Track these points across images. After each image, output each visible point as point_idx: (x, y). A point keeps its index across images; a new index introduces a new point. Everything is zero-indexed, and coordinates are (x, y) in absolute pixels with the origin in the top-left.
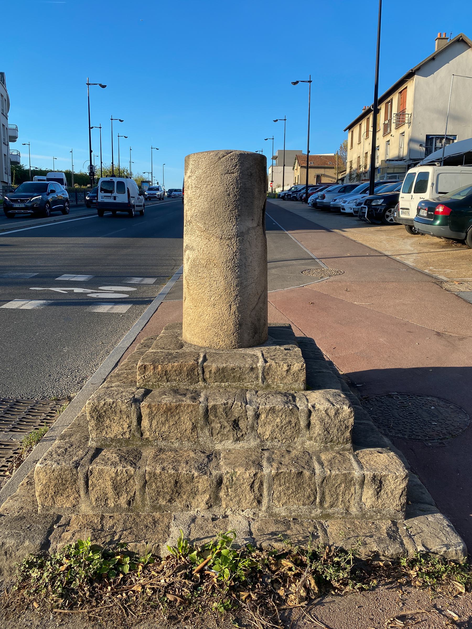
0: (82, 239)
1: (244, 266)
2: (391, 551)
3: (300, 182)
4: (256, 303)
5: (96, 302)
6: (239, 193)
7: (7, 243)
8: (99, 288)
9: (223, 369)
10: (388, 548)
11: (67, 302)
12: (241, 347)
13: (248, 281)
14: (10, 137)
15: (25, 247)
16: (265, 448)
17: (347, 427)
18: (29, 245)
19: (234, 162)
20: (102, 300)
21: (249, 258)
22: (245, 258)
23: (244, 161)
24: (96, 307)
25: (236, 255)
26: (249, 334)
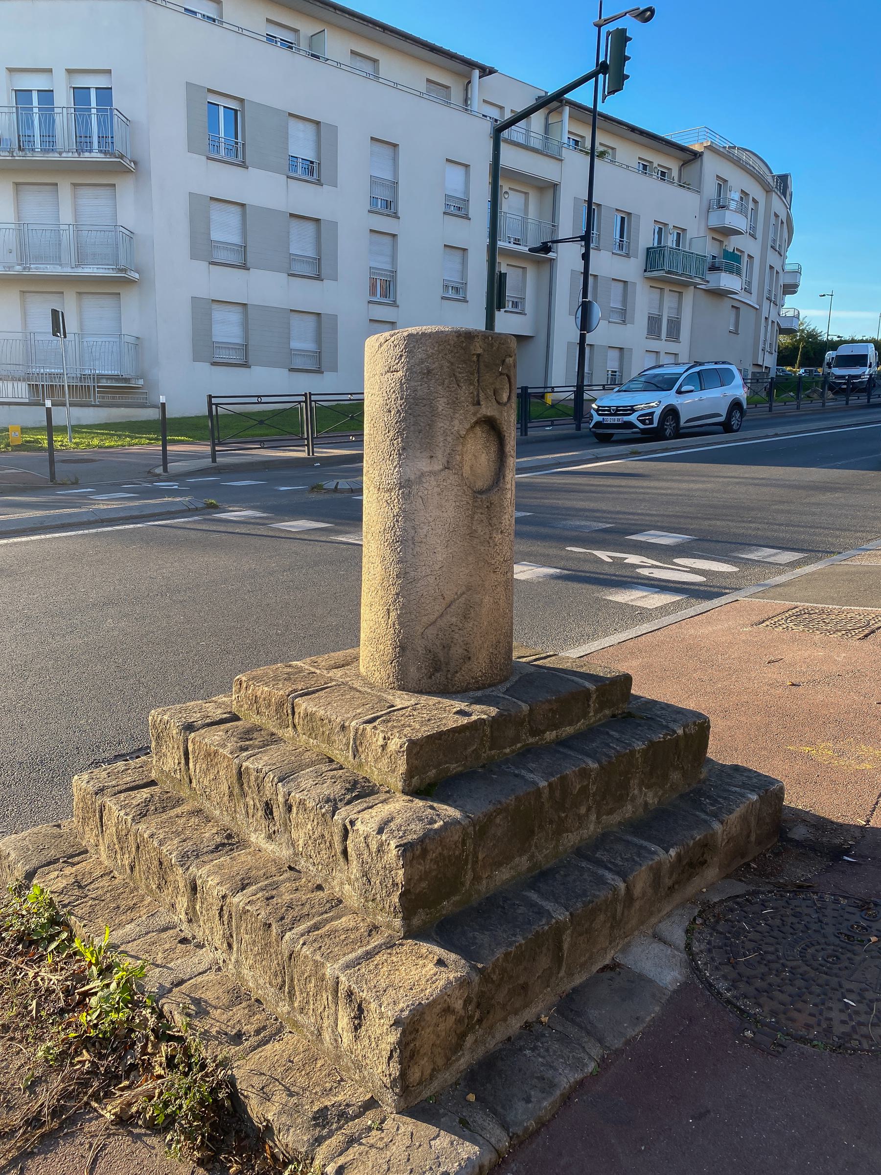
0: (789, 469)
1: (410, 542)
2: (289, 1138)
4: (437, 614)
5: (630, 582)
6: (405, 407)
7: (641, 471)
8: (675, 560)
9: (313, 714)
10: (288, 1130)
11: (585, 577)
12: (403, 689)
14: (785, 286)
15: (667, 480)
16: (297, 868)
17: (395, 884)
18: (669, 478)
19: (398, 350)
20: (646, 582)
21: (422, 529)
22: (414, 528)
23: (414, 347)
25: (397, 521)
26: (419, 669)
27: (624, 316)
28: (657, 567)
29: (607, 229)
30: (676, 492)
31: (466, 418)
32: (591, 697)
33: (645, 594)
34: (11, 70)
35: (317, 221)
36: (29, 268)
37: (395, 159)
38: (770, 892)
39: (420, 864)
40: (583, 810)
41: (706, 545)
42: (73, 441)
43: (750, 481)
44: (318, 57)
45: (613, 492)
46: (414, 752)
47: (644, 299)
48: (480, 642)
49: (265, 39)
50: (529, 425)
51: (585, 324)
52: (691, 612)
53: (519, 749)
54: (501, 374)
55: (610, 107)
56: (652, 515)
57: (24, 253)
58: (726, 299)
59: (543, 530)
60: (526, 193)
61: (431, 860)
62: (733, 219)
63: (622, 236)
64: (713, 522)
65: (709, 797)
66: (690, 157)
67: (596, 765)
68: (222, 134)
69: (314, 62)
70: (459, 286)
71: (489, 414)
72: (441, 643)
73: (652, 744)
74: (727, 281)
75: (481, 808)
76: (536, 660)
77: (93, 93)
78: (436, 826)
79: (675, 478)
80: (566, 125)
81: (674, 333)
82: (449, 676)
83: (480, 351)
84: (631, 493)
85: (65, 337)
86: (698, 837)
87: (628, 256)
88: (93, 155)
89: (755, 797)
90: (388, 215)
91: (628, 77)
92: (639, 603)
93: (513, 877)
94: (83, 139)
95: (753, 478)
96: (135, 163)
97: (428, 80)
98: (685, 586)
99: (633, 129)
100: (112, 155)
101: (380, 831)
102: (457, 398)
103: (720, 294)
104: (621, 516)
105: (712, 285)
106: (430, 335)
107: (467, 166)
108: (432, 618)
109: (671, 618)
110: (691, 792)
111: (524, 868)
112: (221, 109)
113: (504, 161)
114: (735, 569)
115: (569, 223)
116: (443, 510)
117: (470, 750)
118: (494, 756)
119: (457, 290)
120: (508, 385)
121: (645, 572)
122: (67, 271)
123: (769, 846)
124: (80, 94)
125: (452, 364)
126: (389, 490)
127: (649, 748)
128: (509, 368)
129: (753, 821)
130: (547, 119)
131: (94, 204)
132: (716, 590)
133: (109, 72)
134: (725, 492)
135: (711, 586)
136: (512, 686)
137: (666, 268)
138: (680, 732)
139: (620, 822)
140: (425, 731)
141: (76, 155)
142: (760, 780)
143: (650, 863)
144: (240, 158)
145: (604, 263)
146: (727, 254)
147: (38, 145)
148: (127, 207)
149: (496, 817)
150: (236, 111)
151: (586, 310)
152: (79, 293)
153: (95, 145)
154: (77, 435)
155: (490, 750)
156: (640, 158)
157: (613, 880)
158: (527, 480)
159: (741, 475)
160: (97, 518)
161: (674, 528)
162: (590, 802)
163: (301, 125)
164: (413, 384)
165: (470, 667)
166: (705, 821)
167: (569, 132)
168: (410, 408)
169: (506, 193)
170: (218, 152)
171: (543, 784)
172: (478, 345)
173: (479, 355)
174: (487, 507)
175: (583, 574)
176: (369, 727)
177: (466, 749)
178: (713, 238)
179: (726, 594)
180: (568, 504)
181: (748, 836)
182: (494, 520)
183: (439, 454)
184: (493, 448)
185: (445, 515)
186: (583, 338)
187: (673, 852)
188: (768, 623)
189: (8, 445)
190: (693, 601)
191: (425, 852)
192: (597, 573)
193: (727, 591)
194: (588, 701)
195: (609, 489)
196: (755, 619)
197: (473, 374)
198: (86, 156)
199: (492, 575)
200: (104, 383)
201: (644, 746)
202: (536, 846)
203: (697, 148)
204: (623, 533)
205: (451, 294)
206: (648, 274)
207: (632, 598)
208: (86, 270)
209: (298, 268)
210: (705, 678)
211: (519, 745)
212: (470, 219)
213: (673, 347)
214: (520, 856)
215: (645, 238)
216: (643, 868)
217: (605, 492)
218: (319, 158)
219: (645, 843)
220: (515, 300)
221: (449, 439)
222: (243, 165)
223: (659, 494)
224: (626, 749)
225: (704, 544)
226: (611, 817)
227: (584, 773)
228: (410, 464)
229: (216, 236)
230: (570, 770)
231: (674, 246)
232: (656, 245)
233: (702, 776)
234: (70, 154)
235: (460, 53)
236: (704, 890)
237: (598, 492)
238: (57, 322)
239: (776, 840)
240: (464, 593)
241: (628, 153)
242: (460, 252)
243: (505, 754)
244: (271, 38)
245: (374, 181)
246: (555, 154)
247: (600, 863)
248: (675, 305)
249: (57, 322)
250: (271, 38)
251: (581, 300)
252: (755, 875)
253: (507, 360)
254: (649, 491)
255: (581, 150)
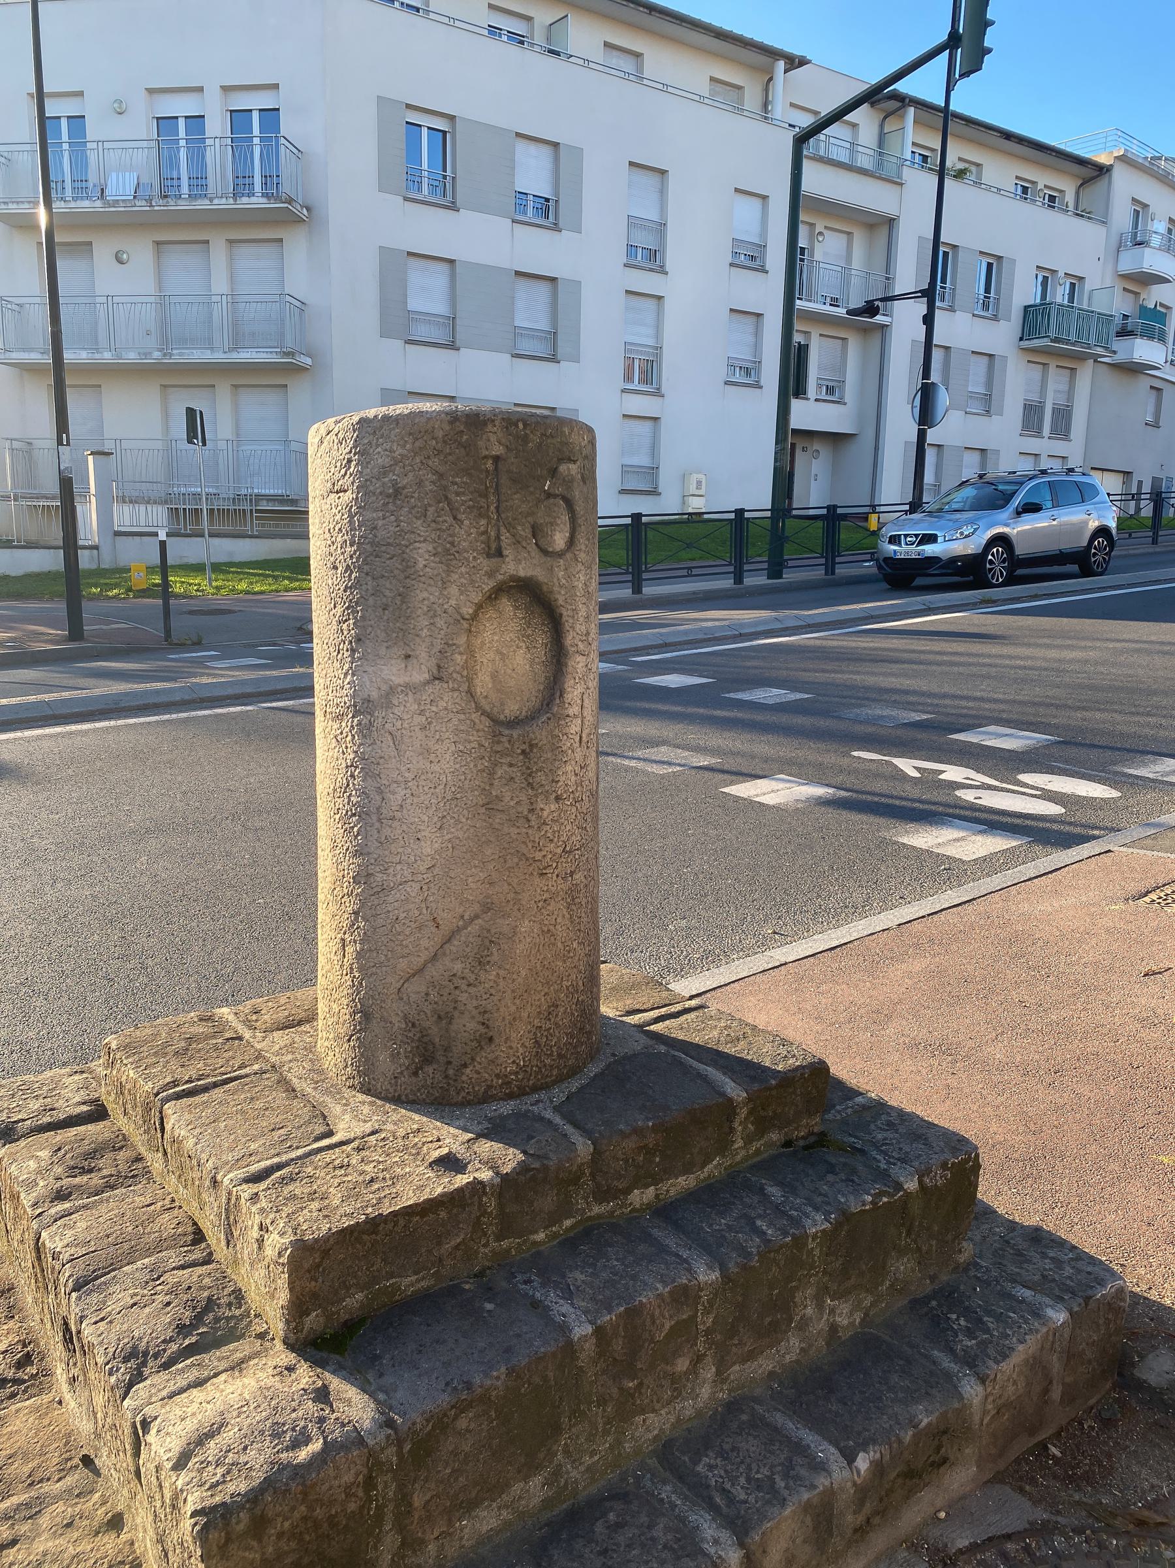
1: (374, 817)
3: (647, 524)
4: (425, 956)
5: (941, 814)
7: (991, 630)
13: (391, 871)
15: (1029, 645)
22: (379, 791)
23: (370, 443)
24: (910, 826)
25: (352, 776)
26: (394, 1056)
27: (988, 404)
28: (995, 788)
29: (967, 278)
30: (1038, 663)
31: (472, 582)
32: (735, 1114)
33: (962, 834)
34: (151, 91)
35: (452, 262)
36: (171, 355)
37: (663, 192)
38: (1079, 1531)
39: (249, 1548)
40: (682, 1364)
41: (1073, 751)
42: (214, 584)
43: (1157, 647)
44: (558, 54)
45: (939, 664)
46: (306, 1266)
47: (1018, 381)
48: (513, 1008)
49: (486, 32)
50: (838, 560)
51: (926, 416)
52: (1030, 870)
53: (567, 1230)
54: (549, 495)
55: (969, 99)
56: (996, 701)
57: (166, 335)
58: (1142, 377)
59: (823, 723)
60: (849, 233)
61: (280, 1535)
62: (1154, 260)
63: (987, 290)
64: (1088, 714)
65: (967, 1312)
66: (1092, 173)
67: (714, 1276)
68: (425, 166)
69: (552, 60)
70: (749, 365)
71: (522, 574)
72: (434, 1011)
73: (846, 1216)
74: (1144, 351)
75: (422, 1399)
76: (657, 1020)
77: (255, 116)
78: (303, 1454)
79: (1040, 641)
80: (911, 133)
81: (1062, 427)
82: (451, 1072)
83: (498, 450)
84: (970, 664)
85: (204, 444)
86: (926, 1421)
87: (995, 318)
88: (253, 200)
89: (1059, 1316)
90: (651, 270)
91: (989, 51)
92: (951, 851)
93: (507, 1524)
94: (240, 181)
95: (1163, 643)
96: (308, 209)
97: (712, 79)
98: (1028, 822)
99: (1008, 136)
100: (278, 199)
101: (180, 1464)
102: (452, 544)
103: (1134, 369)
104: (947, 702)
105: (1120, 357)
106: (397, 420)
107: (764, 198)
108: (417, 962)
109: (996, 881)
110: (934, 1295)
111: (535, 1501)
112: (425, 131)
113: (806, 186)
114: (1115, 794)
115: (909, 273)
116: (437, 757)
117: (448, 1246)
118: (508, 1251)
119: (748, 372)
120: (565, 518)
121: (968, 796)
122: (219, 357)
123: (1092, 1402)
124: (239, 117)
125: (441, 476)
126: (339, 717)
127: (838, 1226)
128: (568, 482)
129: (1056, 1364)
130: (882, 126)
131: (254, 264)
132: (1078, 830)
133: (276, 87)
134: (1114, 664)
135: (1070, 824)
136: (581, 1089)
137: (1052, 334)
138: (912, 1185)
139: (771, 1374)
140: (345, 1212)
141: (231, 201)
142: (1079, 1271)
143: (806, 1496)
144: (449, 198)
145: (954, 328)
146: (1144, 311)
147: (185, 189)
148: (298, 268)
149: (456, 1418)
150: (445, 133)
151: (927, 394)
152: (235, 386)
153: (258, 187)
154: (222, 577)
155: (499, 1238)
156: (1017, 177)
157: (716, 1542)
158: (818, 642)
159: (1145, 638)
160: (195, 696)
161: (1031, 724)
162: (701, 1346)
163: (533, 148)
164: (370, 515)
165: (491, 1056)
166: (948, 1376)
167: (914, 144)
168: (365, 562)
169: (820, 233)
170: (420, 190)
171: (582, 1330)
172: (493, 438)
173: (497, 459)
174: (523, 752)
175: (869, 798)
176: (247, 1190)
177: (439, 1244)
178: (1125, 289)
179: (1095, 838)
180: (871, 680)
181: (1046, 1391)
182: (540, 777)
183: (422, 652)
184: (542, 639)
185: (436, 768)
186: (922, 435)
187: (863, 1463)
188: (1153, 896)
189: (130, 590)
190: (1038, 848)
191: (259, 1524)
192: (892, 797)
193: (1096, 832)
194: (730, 1120)
195: (939, 658)
196: (1134, 887)
197: (486, 496)
198: (245, 202)
199: (537, 880)
200: (264, 506)
201: (827, 1225)
202: (566, 1452)
203: (1103, 159)
204: (945, 729)
205: (738, 377)
206: (1025, 344)
207: (940, 840)
208: (242, 355)
209: (526, 346)
210: (1031, 1001)
211: (568, 1223)
212: (767, 272)
213: (1059, 448)
214: (526, 1479)
215: (1023, 291)
216: (787, 1512)
217: (930, 663)
218: (557, 194)
219: (809, 1437)
220: (830, 384)
221: (440, 623)
222: (453, 207)
223: (1012, 667)
224: (785, 1234)
225: (1072, 751)
226: (751, 1366)
227: (684, 1296)
228: (370, 669)
229: (416, 303)
230: (651, 1292)
231: (1066, 302)
232: (1038, 301)
233: (962, 1258)
234: (224, 201)
235: (758, 38)
236: (942, 1515)
237: (921, 663)
238: (194, 425)
239: (1109, 1385)
240: (477, 917)
241: (1000, 172)
242: (753, 319)
243: (535, 1243)
244: (494, 31)
245: (633, 222)
246: (892, 174)
247: (700, 1492)
248: (1064, 387)
249: (194, 425)
250: (494, 31)
251: (920, 381)
252: (1055, 1477)
253: (563, 468)
254: (998, 661)
255: (930, 169)
